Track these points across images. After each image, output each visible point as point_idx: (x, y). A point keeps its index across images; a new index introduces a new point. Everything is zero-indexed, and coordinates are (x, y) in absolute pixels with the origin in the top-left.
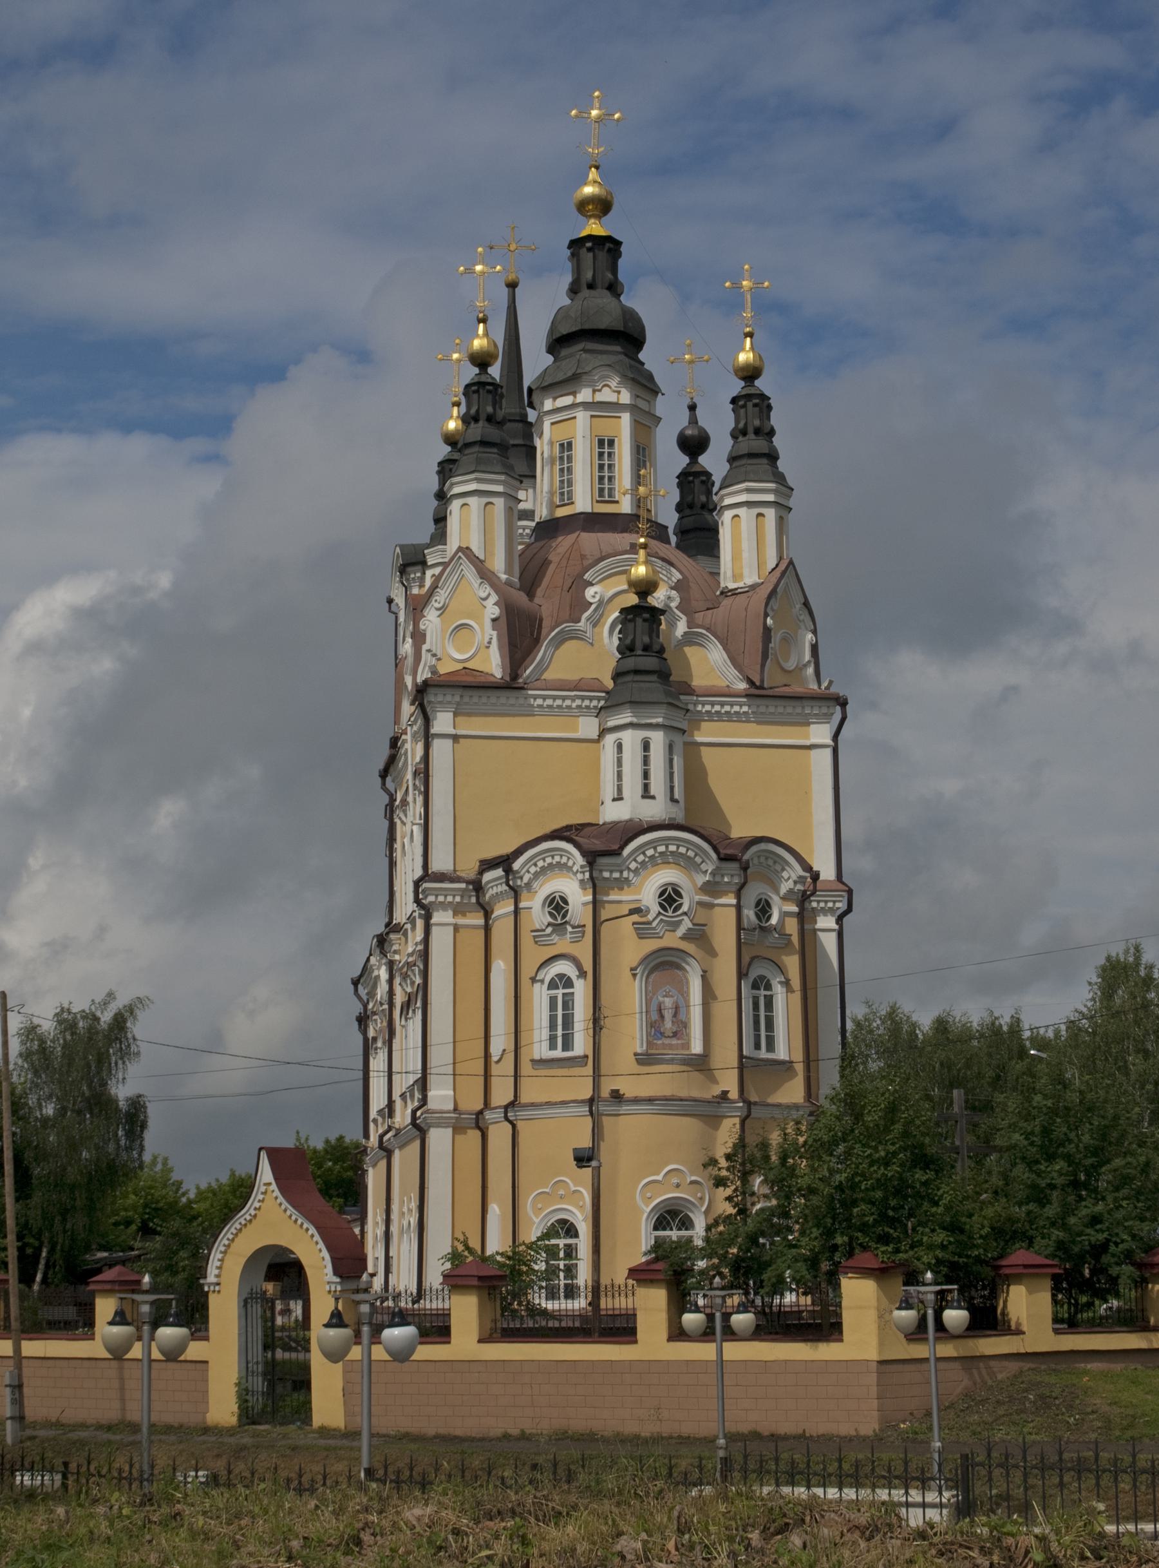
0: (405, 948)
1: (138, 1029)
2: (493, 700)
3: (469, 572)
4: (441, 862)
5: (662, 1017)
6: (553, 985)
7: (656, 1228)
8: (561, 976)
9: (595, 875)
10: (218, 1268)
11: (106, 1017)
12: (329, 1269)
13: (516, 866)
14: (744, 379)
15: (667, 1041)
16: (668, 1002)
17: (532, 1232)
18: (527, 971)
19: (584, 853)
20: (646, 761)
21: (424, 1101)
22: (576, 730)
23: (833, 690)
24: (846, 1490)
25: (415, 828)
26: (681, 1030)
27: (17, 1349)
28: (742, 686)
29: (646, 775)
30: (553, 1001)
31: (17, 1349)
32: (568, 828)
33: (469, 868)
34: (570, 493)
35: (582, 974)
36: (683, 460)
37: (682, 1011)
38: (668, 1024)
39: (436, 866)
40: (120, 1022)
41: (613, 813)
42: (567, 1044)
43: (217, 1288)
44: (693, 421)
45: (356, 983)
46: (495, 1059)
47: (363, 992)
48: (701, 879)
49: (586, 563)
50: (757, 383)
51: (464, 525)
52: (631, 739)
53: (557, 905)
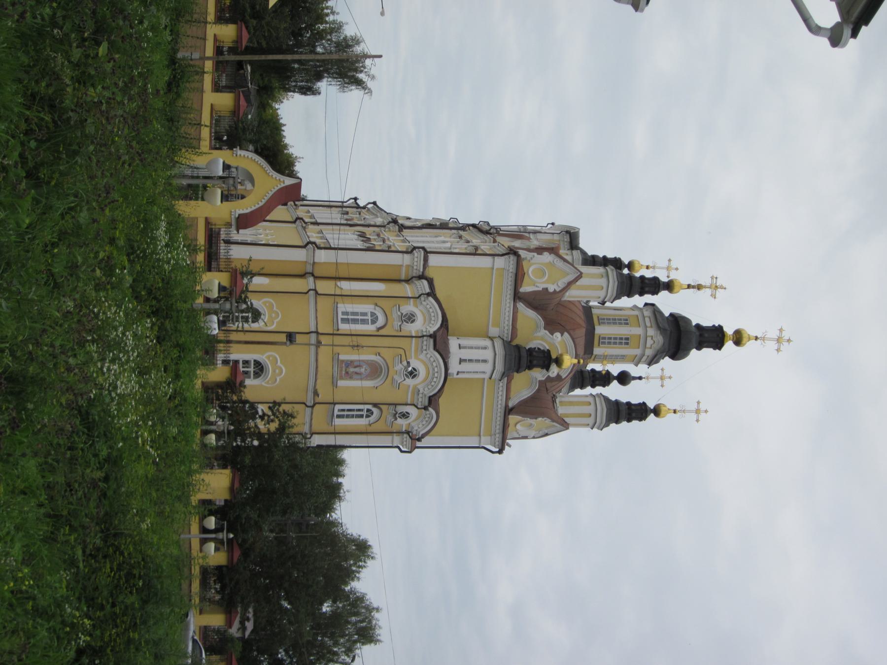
0: (393, 239)
1: (355, 93)
2: (509, 292)
3: (571, 278)
4: (433, 260)
5: (356, 367)
6: (373, 314)
7: (255, 361)
8: (377, 318)
9: (425, 338)
11: (361, 76)
12: (242, 212)
13: (431, 299)
14: (655, 408)
16: (363, 370)
17: (257, 302)
18: (381, 302)
19: (435, 332)
20: (478, 361)
21: (320, 248)
22: (493, 326)
23: (506, 447)
24: (206, 70)
25: (448, 245)
26: (349, 376)
27: (209, 58)
28: (511, 405)
29: (470, 361)
30: (365, 314)
31: (209, 58)
32: (447, 329)
33: (430, 273)
34: (604, 323)
35: (379, 329)
36: (615, 374)
37: (359, 377)
38: (352, 370)
39: (431, 256)
40: (359, 83)
41: (453, 343)
42: (345, 321)
44: (635, 378)
45: (374, 203)
46: (338, 283)
47: (370, 206)
48: (421, 388)
49: (571, 332)
50: (652, 415)
51: (592, 276)
53: (410, 318)
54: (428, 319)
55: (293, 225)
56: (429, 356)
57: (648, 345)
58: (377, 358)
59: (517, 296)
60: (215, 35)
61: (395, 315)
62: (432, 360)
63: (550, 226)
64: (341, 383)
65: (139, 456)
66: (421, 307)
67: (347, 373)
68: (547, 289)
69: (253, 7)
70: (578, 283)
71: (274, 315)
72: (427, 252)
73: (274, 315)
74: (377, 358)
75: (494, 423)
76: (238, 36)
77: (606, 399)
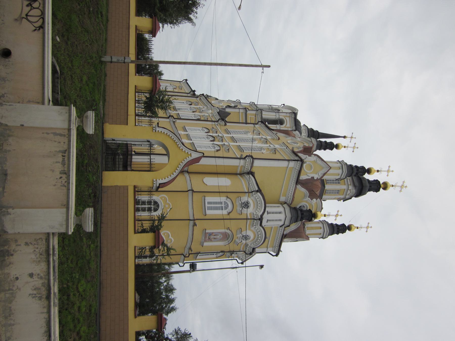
6: (225, 203)
10: (161, 132)
11: (191, 16)
13: (259, 194)
15: (208, 237)
18: (229, 195)
26: (210, 240)
28: (285, 233)
29: (273, 220)
30: (221, 203)
33: (253, 170)
40: (190, 20)
43: (154, 131)
52: (282, 216)
54: (257, 206)
55: (168, 120)
56: (256, 229)
57: (348, 194)
58: (228, 231)
59: (298, 181)
60: (136, 26)
61: (238, 203)
62: (258, 230)
63: (282, 106)
64: (206, 244)
65: (77, 46)
66: (252, 198)
67: (209, 238)
68: (313, 177)
69: (161, 2)
70: (328, 173)
71: (167, 206)
72: (253, 159)
73: (167, 206)
74: (228, 231)
75: (275, 242)
76: (153, 28)
77: (327, 223)
